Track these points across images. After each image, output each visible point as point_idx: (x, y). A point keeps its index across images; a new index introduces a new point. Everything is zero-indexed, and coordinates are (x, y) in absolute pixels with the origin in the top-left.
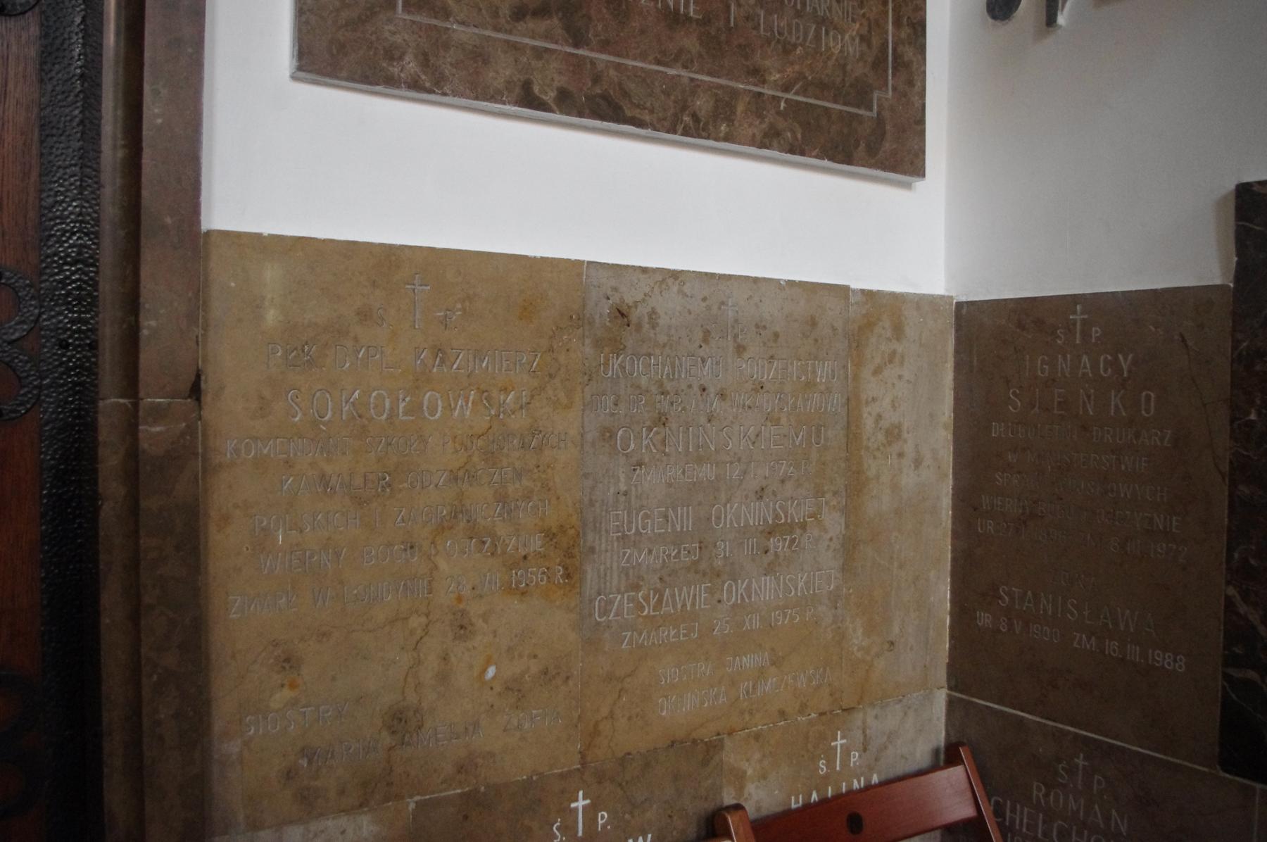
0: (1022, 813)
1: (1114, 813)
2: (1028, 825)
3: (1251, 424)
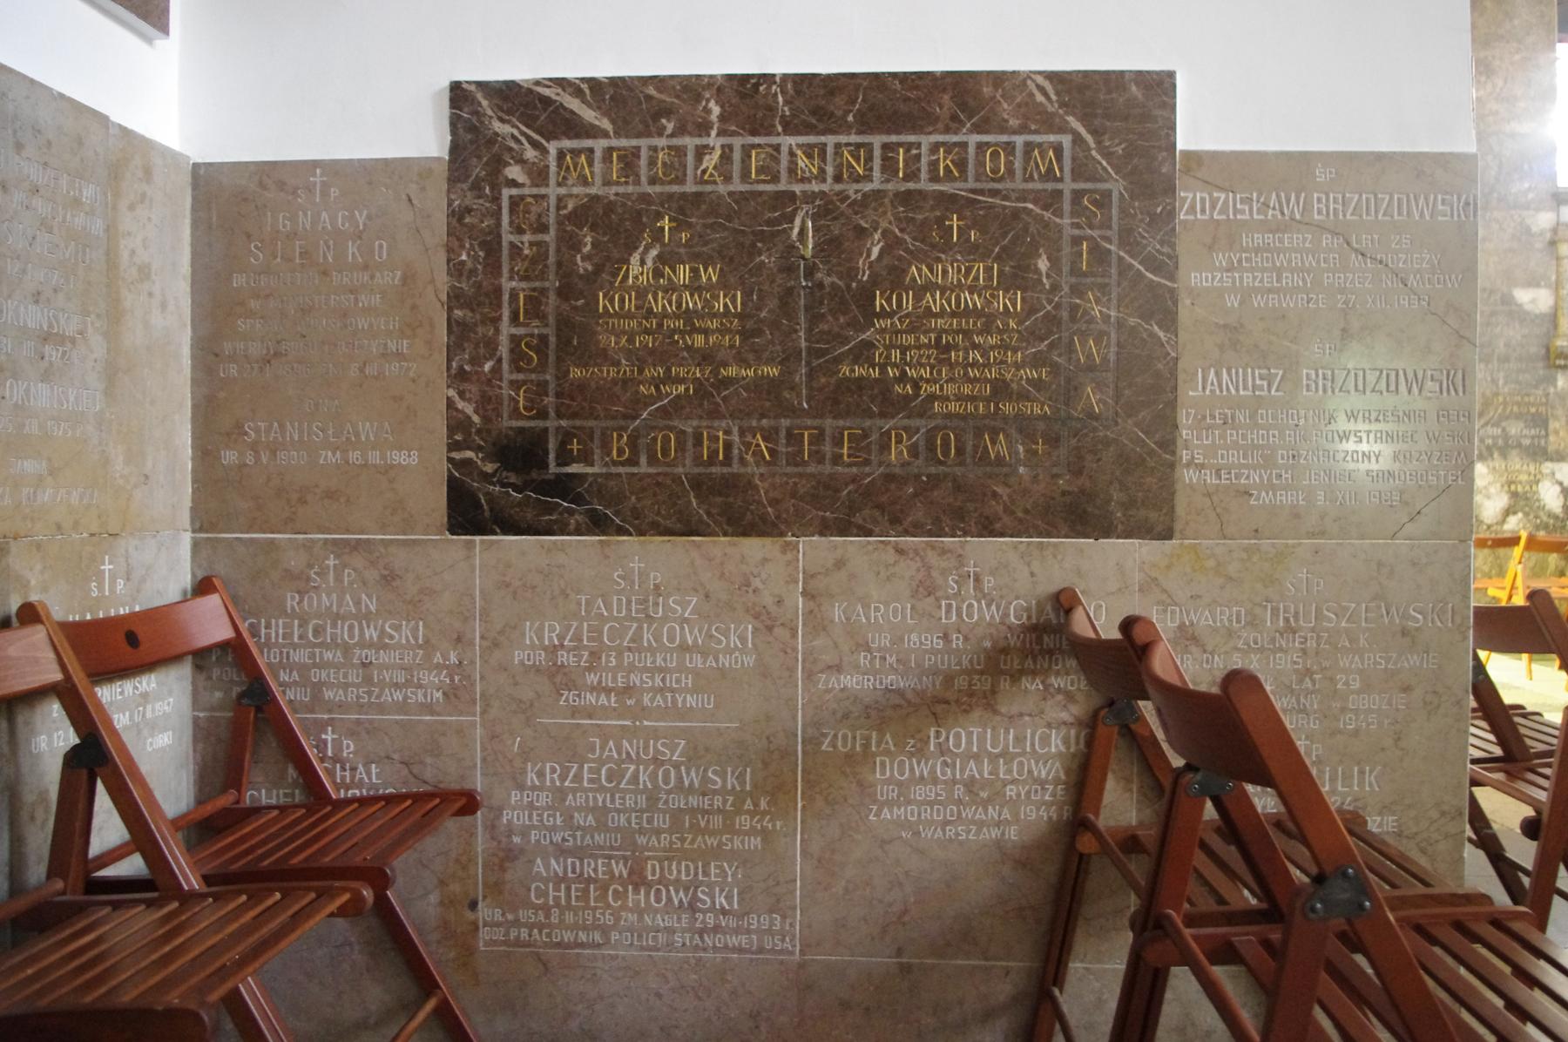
0: (277, 626)
1: (364, 596)
2: (284, 634)
3: (463, 262)
